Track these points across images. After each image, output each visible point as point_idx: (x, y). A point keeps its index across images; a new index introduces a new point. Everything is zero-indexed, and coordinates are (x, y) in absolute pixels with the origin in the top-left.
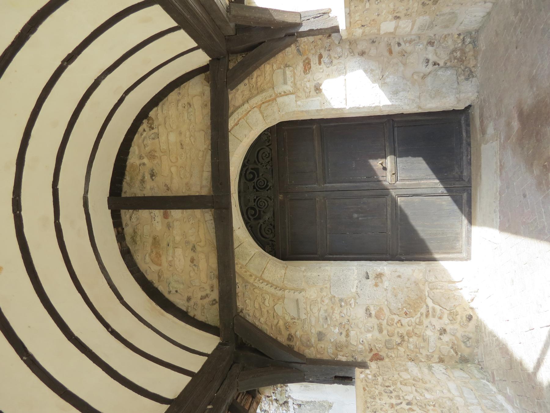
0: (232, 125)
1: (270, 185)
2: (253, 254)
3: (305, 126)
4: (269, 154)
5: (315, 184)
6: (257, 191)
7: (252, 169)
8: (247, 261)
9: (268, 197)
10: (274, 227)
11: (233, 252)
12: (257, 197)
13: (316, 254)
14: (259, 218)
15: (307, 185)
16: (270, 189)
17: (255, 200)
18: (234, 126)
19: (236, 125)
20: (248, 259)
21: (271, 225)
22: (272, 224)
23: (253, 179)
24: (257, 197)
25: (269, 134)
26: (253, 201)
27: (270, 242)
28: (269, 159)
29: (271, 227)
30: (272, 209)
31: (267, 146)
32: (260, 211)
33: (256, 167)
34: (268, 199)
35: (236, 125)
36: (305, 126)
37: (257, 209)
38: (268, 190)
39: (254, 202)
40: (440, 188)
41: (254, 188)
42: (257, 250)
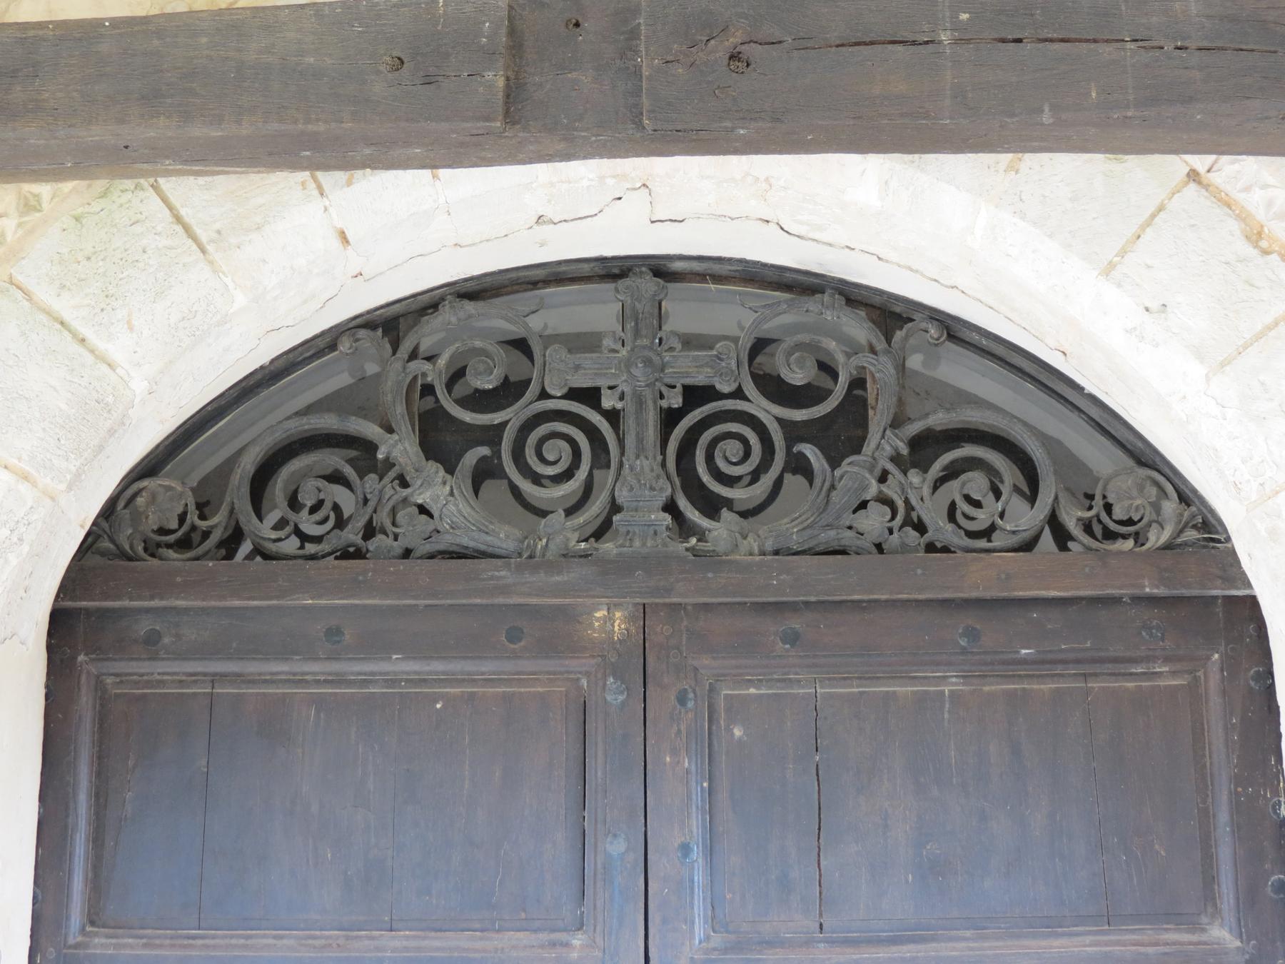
0: (1254, 202)
1: (721, 530)
2: (117, 355)
3: (1225, 853)
4: (988, 533)
5: (715, 922)
6: (670, 418)
7: (858, 383)
8: (45, 294)
9: (615, 508)
10: (346, 554)
11: (119, 160)
12: (613, 417)
13: (93, 918)
14: (438, 440)
15: (710, 851)
16: (683, 527)
17: (590, 396)
18: (1243, 217)
19: (1255, 236)
20: (64, 306)
21: (370, 531)
22: (379, 541)
23: (775, 389)
24: (613, 417)
25: (1157, 538)
26: (582, 381)
27: (218, 520)
28: (941, 530)
29: (352, 535)
30: (503, 537)
31: (1054, 521)
32: (492, 435)
33: (878, 419)
34: (596, 507)
35: (1255, 236)
36: (1225, 853)
37: (512, 416)
38: (670, 507)
39: (574, 394)
40: (1214, 157)
41: (696, 395)
42: (139, 386)
